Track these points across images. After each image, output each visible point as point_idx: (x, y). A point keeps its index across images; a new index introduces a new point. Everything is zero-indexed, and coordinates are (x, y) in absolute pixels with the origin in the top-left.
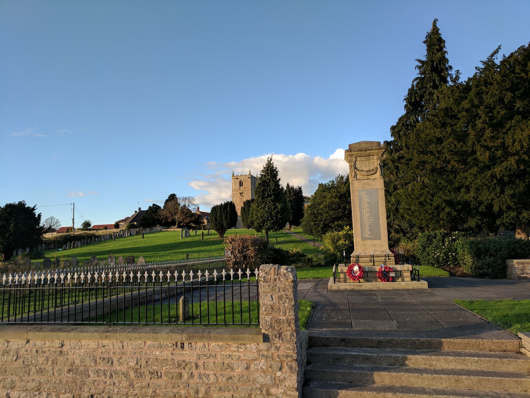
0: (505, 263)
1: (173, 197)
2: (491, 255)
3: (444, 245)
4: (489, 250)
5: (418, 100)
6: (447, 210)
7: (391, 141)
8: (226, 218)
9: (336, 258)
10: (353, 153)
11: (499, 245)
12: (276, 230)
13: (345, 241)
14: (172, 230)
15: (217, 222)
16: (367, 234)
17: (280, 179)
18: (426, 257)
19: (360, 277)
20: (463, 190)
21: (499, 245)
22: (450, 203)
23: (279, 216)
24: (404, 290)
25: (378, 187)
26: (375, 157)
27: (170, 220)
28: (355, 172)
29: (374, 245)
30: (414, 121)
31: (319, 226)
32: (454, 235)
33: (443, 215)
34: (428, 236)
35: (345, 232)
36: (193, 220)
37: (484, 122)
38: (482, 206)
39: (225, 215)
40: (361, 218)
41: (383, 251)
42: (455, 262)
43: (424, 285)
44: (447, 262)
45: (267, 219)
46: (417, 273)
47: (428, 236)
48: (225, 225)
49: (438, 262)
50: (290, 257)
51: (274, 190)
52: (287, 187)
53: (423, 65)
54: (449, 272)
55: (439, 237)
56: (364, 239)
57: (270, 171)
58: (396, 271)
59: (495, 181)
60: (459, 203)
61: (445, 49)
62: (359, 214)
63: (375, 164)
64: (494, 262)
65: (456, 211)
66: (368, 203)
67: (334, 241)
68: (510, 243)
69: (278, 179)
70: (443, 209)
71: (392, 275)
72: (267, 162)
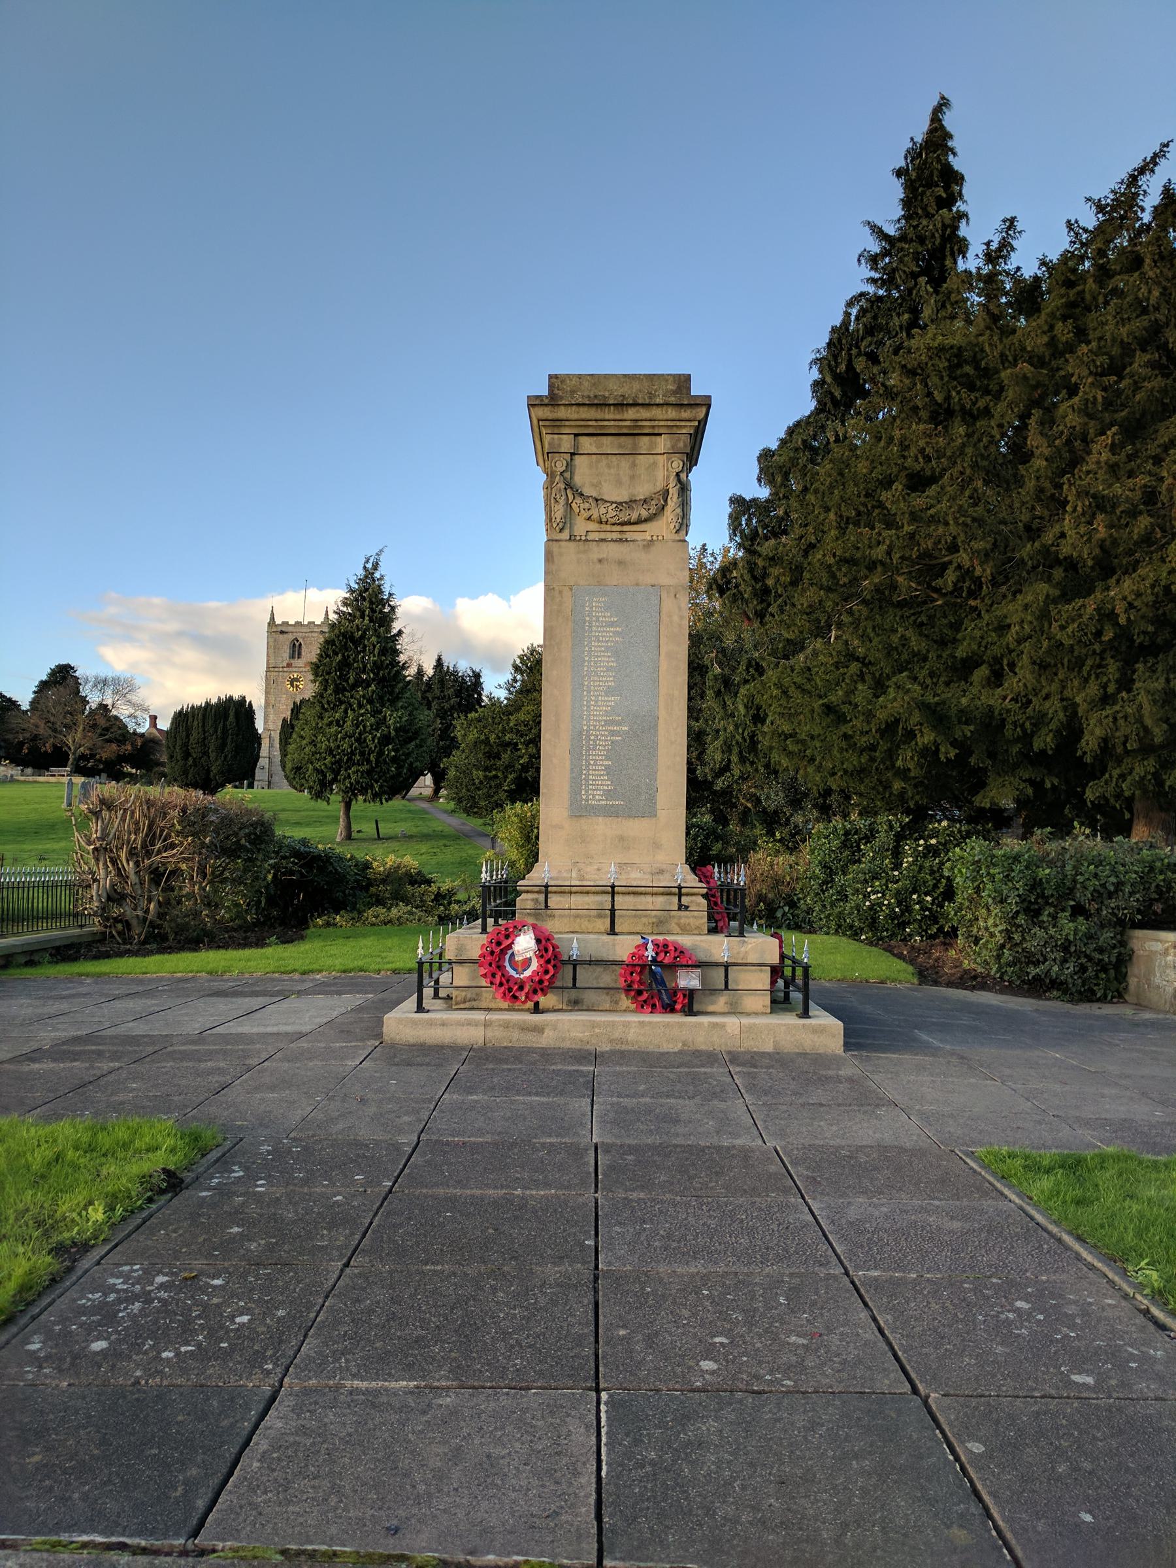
0: (1123, 944)
1: (63, 676)
2: (1079, 911)
3: (897, 866)
4: (1072, 890)
6: (926, 737)
7: (754, 500)
8: (221, 748)
10: (562, 413)
11: (1114, 871)
12: (376, 796)
14: (52, 779)
16: (598, 788)
18: (832, 904)
19: (540, 986)
20: (982, 672)
21: (1114, 871)
22: (937, 716)
24: (734, 1058)
25: (665, 580)
26: (662, 444)
27: (48, 748)
28: (569, 505)
30: (837, 435)
31: (499, 786)
32: (935, 834)
33: (906, 758)
36: (118, 752)
37: (1087, 411)
38: (1044, 731)
39: (216, 739)
41: (661, 872)
42: (929, 927)
43: (823, 1031)
44: (903, 925)
45: (350, 759)
46: (799, 981)
47: (847, 833)
48: (214, 770)
49: (873, 924)
50: (370, 883)
51: (377, 667)
52: (436, 667)
54: (912, 962)
55: (884, 837)
56: (580, 810)
57: (370, 607)
59: (1108, 635)
60: (965, 716)
61: (960, 206)
63: (660, 474)
64: (1090, 937)
65: (954, 744)
68: (1152, 869)
69: (394, 632)
70: (910, 735)
71: (688, 980)
72: (361, 573)
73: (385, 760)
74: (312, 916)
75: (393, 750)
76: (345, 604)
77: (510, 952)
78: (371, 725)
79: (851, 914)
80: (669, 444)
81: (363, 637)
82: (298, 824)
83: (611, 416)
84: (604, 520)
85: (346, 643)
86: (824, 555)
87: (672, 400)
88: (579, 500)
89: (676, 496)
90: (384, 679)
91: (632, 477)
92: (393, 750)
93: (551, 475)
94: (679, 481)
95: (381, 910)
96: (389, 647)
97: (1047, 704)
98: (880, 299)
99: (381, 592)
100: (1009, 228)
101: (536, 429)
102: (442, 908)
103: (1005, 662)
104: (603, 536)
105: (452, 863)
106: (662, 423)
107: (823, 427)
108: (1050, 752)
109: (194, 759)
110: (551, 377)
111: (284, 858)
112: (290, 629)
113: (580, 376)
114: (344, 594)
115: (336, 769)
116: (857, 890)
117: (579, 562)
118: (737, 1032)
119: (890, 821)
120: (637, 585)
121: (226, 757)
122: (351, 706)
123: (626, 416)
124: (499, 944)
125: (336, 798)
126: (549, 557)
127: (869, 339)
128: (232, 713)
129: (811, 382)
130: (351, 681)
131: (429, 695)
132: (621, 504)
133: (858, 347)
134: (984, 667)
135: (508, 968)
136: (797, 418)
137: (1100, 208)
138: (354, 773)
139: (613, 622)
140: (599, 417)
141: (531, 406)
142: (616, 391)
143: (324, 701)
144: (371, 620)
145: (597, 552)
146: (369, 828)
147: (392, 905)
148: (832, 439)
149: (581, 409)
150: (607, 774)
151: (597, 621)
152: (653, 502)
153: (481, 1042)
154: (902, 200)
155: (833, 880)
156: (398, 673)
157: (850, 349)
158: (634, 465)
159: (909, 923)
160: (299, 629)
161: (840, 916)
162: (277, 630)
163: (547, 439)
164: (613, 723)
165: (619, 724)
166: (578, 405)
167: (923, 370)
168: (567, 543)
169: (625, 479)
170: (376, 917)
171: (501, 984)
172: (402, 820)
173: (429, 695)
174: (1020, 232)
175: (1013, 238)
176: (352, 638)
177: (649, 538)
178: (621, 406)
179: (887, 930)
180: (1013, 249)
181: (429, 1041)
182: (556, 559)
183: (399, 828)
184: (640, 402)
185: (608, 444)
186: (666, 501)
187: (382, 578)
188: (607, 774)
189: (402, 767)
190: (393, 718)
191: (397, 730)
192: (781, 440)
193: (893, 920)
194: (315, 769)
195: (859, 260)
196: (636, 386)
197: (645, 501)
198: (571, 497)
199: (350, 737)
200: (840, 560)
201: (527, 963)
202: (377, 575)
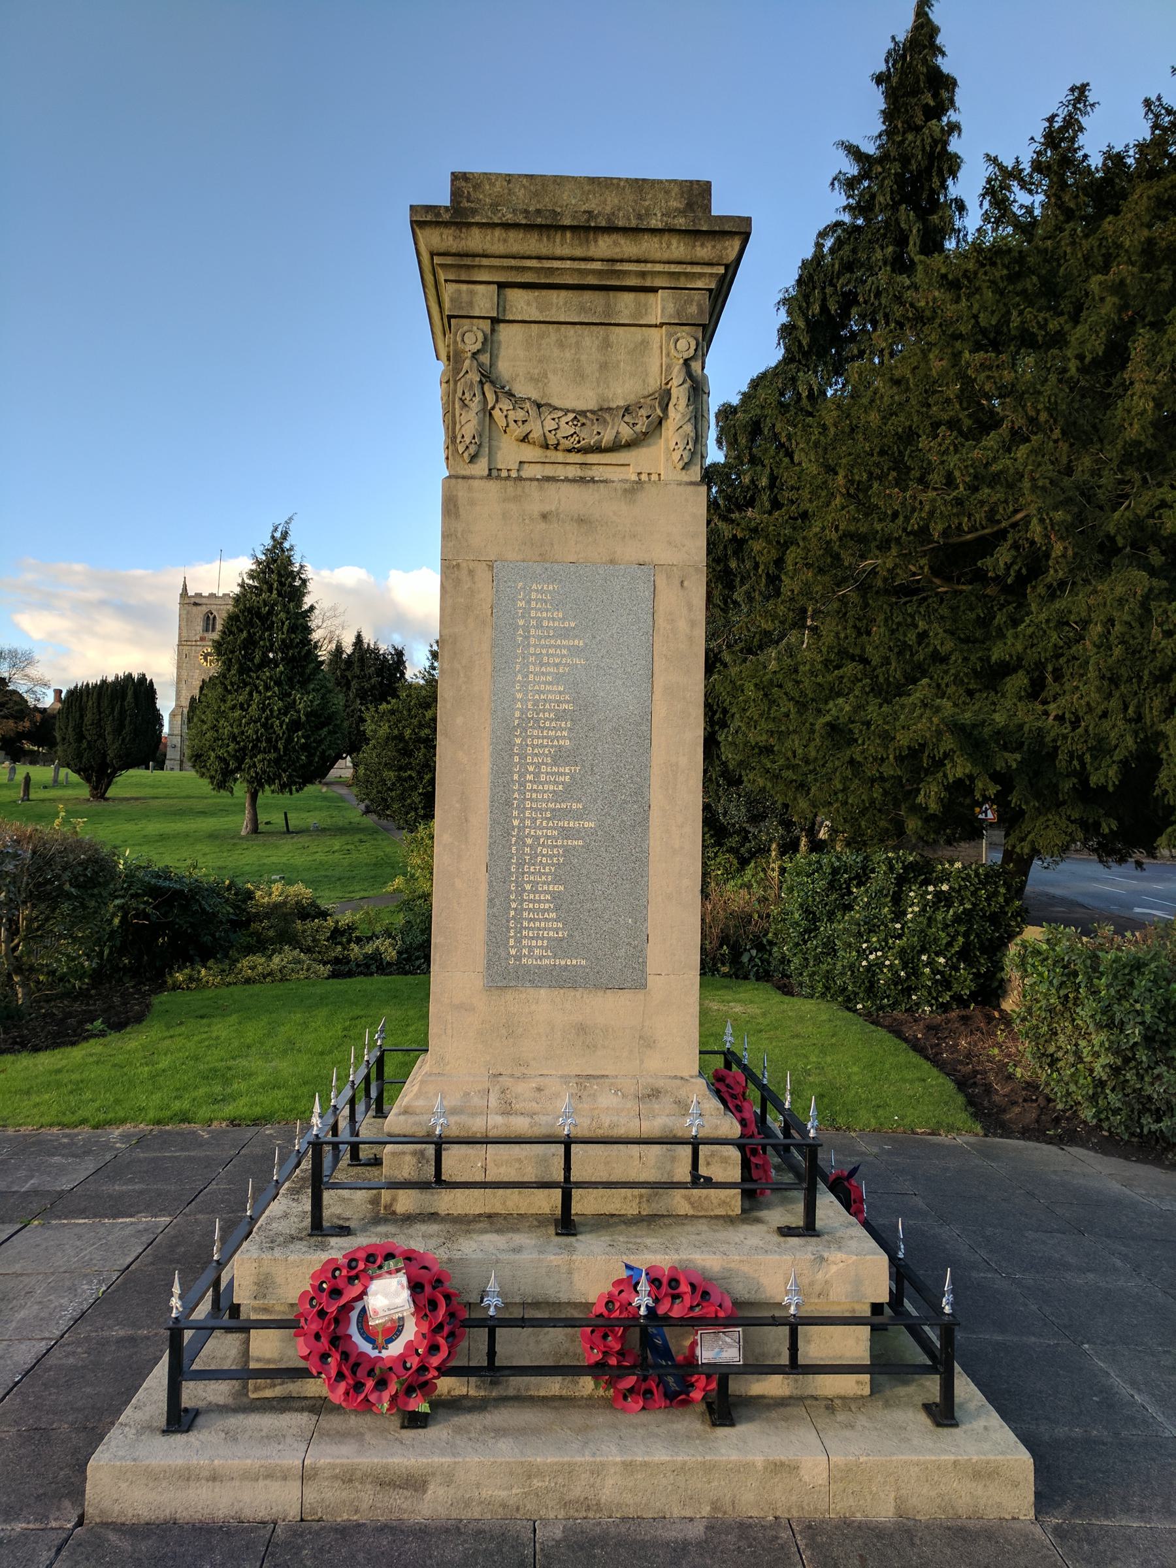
3: (899, 915)
5: (833, 308)
8: (118, 731)
10: (475, 240)
12: (283, 787)
15: (85, 745)
16: (538, 938)
17: (312, 608)
18: (818, 961)
20: (1018, 681)
23: (299, 738)
25: (662, 554)
26: (659, 307)
28: (487, 413)
29: (584, 1035)
30: (811, 389)
31: (415, 788)
34: (835, 871)
40: (502, 805)
44: (908, 991)
45: (255, 746)
47: (835, 871)
48: (111, 754)
49: (871, 990)
50: (257, 917)
51: (285, 646)
53: (864, 175)
55: (880, 878)
56: (504, 975)
57: (278, 580)
58: (745, 1315)
60: (1007, 739)
62: (485, 769)
63: (654, 364)
69: (306, 607)
71: (719, 1349)
72: (269, 543)
73: (294, 747)
74: (171, 968)
75: (303, 737)
76: (251, 577)
77: (359, 1306)
78: (279, 710)
79: (843, 974)
80: (671, 308)
81: (270, 613)
82: (203, 813)
83: (566, 251)
84: (552, 441)
85: (251, 619)
86: (823, 529)
87: (681, 222)
88: (505, 404)
89: (683, 402)
90: (293, 658)
91: (604, 366)
92: (303, 737)
93: (454, 359)
94: (689, 374)
95: (259, 959)
96: (300, 623)
97: (1106, 724)
98: (857, 229)
99: (292, 564)
100: (1077, 101)
101: (429, 278)
102: (339, 948)
103: (1050, 668)
104: (549, 471)
105: (366, 864)
106: (659, 268)
107: (794, 380)
108: (1111, 789)
109: (89, 742)
110: (455, 177)
111: (135, 896)
112: (204, 601)
113: (509, 178)
114: (248, 564)
115: (240, 756)
116: (850, 945)
117: (505, 516)
118: (822, 1479)
119: (889, 860)
120: (612, 562)
121: (123, 740)
122: (257, 687)
123: (593, 251)
124: (336, 1292)
125: (240, 789)
126: (450, 507)
127: (848, 275)
128: (130, 693)
129: (778, 326)
130: (257, 660)
131: (348, 673)
132: (583, 413)
133: (832, 285)
134: (1021, 673)
135: (357, 1338)
136: (762, 370)
138: (260, 761)
140: (544, 251)
141: (417, 225)
142: (571, 205)
143: (227, 682)
144: (279, 594)
145: (538, 500)
146: (277, 819)
147: (274, 951)
148: (805, 394)
149: (512, 235)
151: (539, 626)
152: (643, 412)
153: (293, 1513)
154: (883, 112)
155: (817, 929)
156: (310, 652)
157: (824, 288)
158: (606, 344)
159: (916, 989)
160: (213, 601)
161: (828, 976)
162: (190, 601)
163: (448, 291)
164: (567, 814)
165: (579, 816)
166: (507, 226)
167: (970, 281)
168: (483, 483)
169: (591, 369)
170: (253, 968)
171: (340, 1376)
172: (316, 809)
173: (348, 673)
174: (1092, 105)
176: (258, 615)
177: (634, 477)
178: (586, 230)
179: (888, 997)
180: (1081, 129)
181: (183, 1515)
183: (313, 819)
184: (621, 224)
185: (560, 305)
186: (665, 409)
187: (291, 549)
188: (557, 909)
189: (313, 755)
190: (303, 702)
191: (307, 715)
192: (744, 394)
193: (896, 985)
194: (218, 757)
195: (832, 184)
196: (612, 200)
197: (627, 410)
199: (255, 722)
200: (844, 535)
201: (394, 1330)
202: (286, 545)
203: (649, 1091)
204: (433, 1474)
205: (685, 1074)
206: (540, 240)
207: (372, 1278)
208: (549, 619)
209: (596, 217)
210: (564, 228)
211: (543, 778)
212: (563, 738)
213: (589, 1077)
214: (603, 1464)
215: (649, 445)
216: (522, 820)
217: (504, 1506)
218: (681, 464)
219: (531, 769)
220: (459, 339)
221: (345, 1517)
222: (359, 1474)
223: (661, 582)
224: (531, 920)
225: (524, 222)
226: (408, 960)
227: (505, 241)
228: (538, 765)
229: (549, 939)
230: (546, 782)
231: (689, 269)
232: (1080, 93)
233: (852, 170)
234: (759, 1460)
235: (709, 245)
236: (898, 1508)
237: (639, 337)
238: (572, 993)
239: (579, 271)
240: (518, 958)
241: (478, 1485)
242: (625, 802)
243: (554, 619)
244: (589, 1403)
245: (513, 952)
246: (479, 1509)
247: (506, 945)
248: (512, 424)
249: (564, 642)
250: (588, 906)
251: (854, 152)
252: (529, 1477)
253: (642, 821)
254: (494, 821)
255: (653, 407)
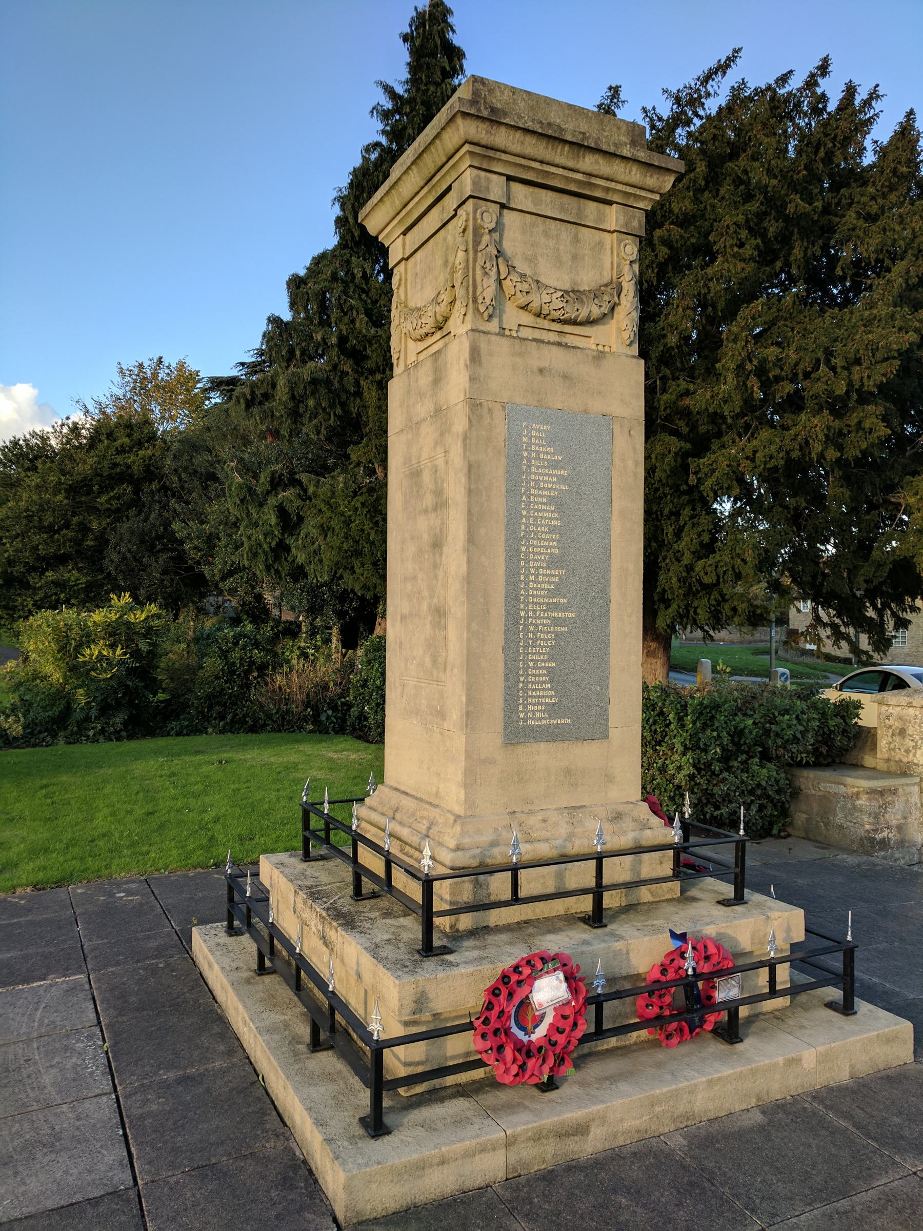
9: (69, 708)
13: (113, 646)
25: (617, 410)
26: (613, 217)
35: (114, 617)
53: (397, 110)
62: (501, 571)
66: (559, 503)
67: (68, 647)
91: (575, 257)
100: (613, 97)
104: (537, 334)
106: (620, 187)
113: (514, 90)
132: (567, 292)
136: (321, 251)
137: (678, 100)
139: (557, 461)
150: (550, 681)
154: (408, 64)
158: (576, 240)
165: (564, 608)
166: (526, 131)
169: (566, 258)
175: (618, 107)
178: (579, 147)
181: (421, 1198)
182: (483, 359)
184: (604, 147)
185: (548, 202)
188: (550, 681)
195: (372, 112)
198: (503, 269)
203: (614, 815)
204: (593, 1120)
205: (633, 800)
206: (547, 148)
207: (535, 979)
208: (544, 453)
209: (588, 138)
210: (566, 142)
211: (541, 578)
212: (554, 547)
213: (574, 808)
214: (695, 1085)
215: (604, 324)
216: (527, 612)
217: (638, 1131)
218: (628, 342)
219: (532, 571)
220: (478, 216)
221: (536, 1168)
222: (544, 1133)
223: (617, 430)
224: (534, 690)
225: (540, 131)
226: (31, 733)
227: (522, 143)
228: (537, 569)
229: (546, 704)
230: (544, 582)
231: (638, 192)
232: (615, 91)
233: (388, 105)
234: (780, 1060)
235: (655, 177)
236: (851, 1072)
237: (597, 239)
238: (561, 745)
239: (567, 178)
240: (525, 720)
241: (622, 1120)
242: (595, 598)
243: (547, 453)
244: (642, 1046)
245: (522, 715)
246: (622, 1138)
247: (517, 711)
248: (518, 293)
249: (555, 472)
250: (571, 677)
251: (389, 91)
252: (653, 1106)
253: (605, 614)
254: (508, 613)
255: (612, 295)
